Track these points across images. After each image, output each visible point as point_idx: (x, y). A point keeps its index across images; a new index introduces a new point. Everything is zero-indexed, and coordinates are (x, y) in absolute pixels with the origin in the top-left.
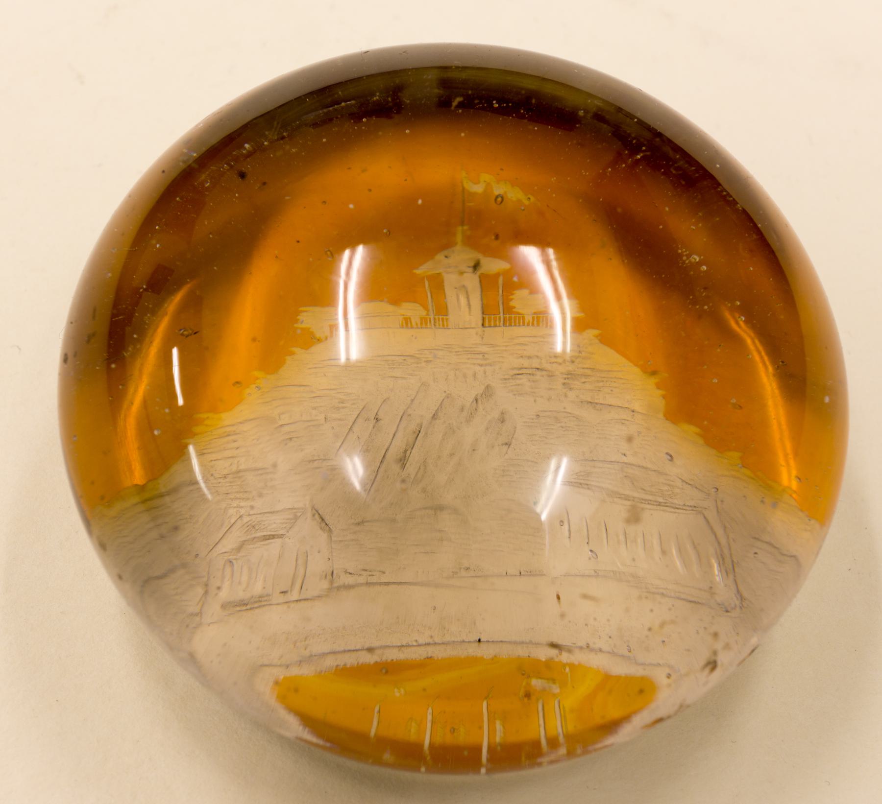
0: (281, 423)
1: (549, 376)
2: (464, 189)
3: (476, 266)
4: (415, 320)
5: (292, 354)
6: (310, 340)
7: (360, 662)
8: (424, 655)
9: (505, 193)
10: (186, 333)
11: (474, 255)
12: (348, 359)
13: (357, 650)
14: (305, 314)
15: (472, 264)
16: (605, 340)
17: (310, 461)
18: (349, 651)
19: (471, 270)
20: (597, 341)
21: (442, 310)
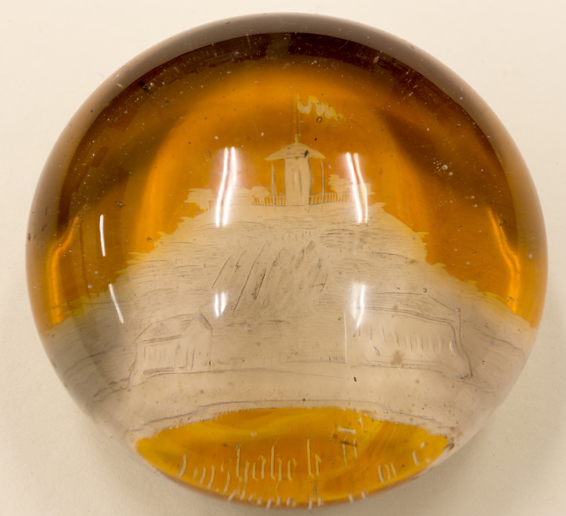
0: (177, 265)
1: (350, 234)
2: (297, 110)
3: (306, 153)
4: (262, 200)
5: (182, 221)
6: (195, 211)
7: (230, 411)
8: (270, 406)
9: (324, 114)
10: (121, 204)
11: (305, 148)
12: (221, 224)
13: (228, 403)
14: (192, 193)
15: (304, 152)
16: (387, 209)
17: (196, 290)
18: (223, 403)
19: (303, 155)
20: (383, 211)
21: (281, 190)
